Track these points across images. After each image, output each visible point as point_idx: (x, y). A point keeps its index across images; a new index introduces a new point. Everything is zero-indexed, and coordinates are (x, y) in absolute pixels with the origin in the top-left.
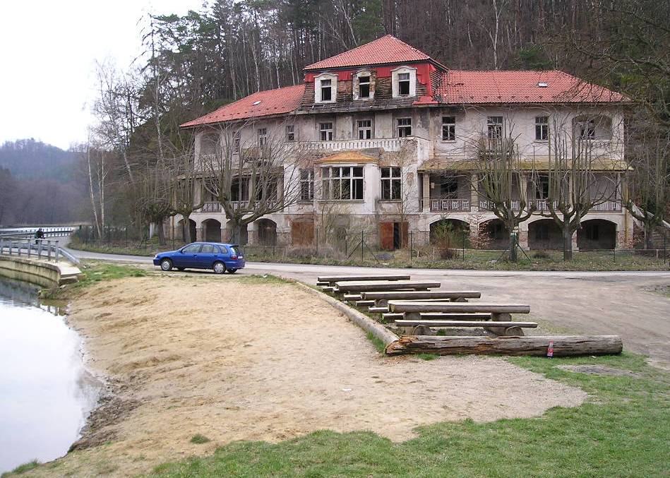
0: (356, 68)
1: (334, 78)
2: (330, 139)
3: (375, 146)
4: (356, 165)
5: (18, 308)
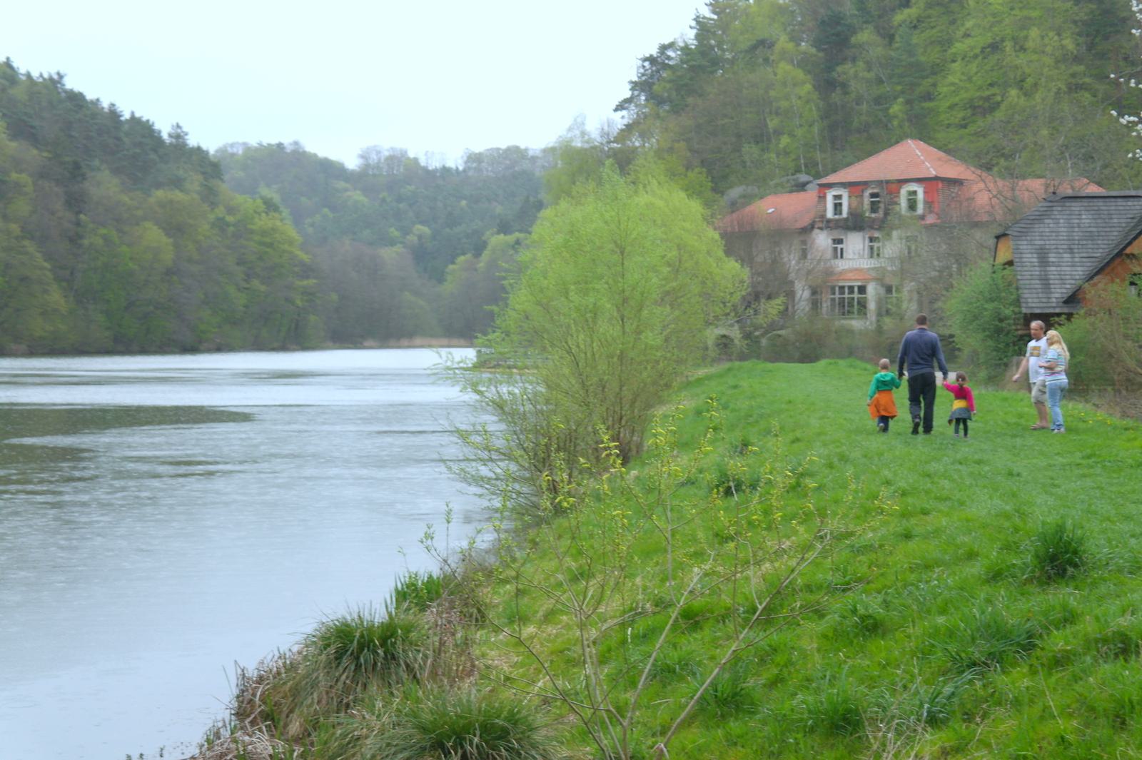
0: (865, 184)
1: (845, 194)
2: (842, 257)
4: (860, 284)
5: (523, 147)
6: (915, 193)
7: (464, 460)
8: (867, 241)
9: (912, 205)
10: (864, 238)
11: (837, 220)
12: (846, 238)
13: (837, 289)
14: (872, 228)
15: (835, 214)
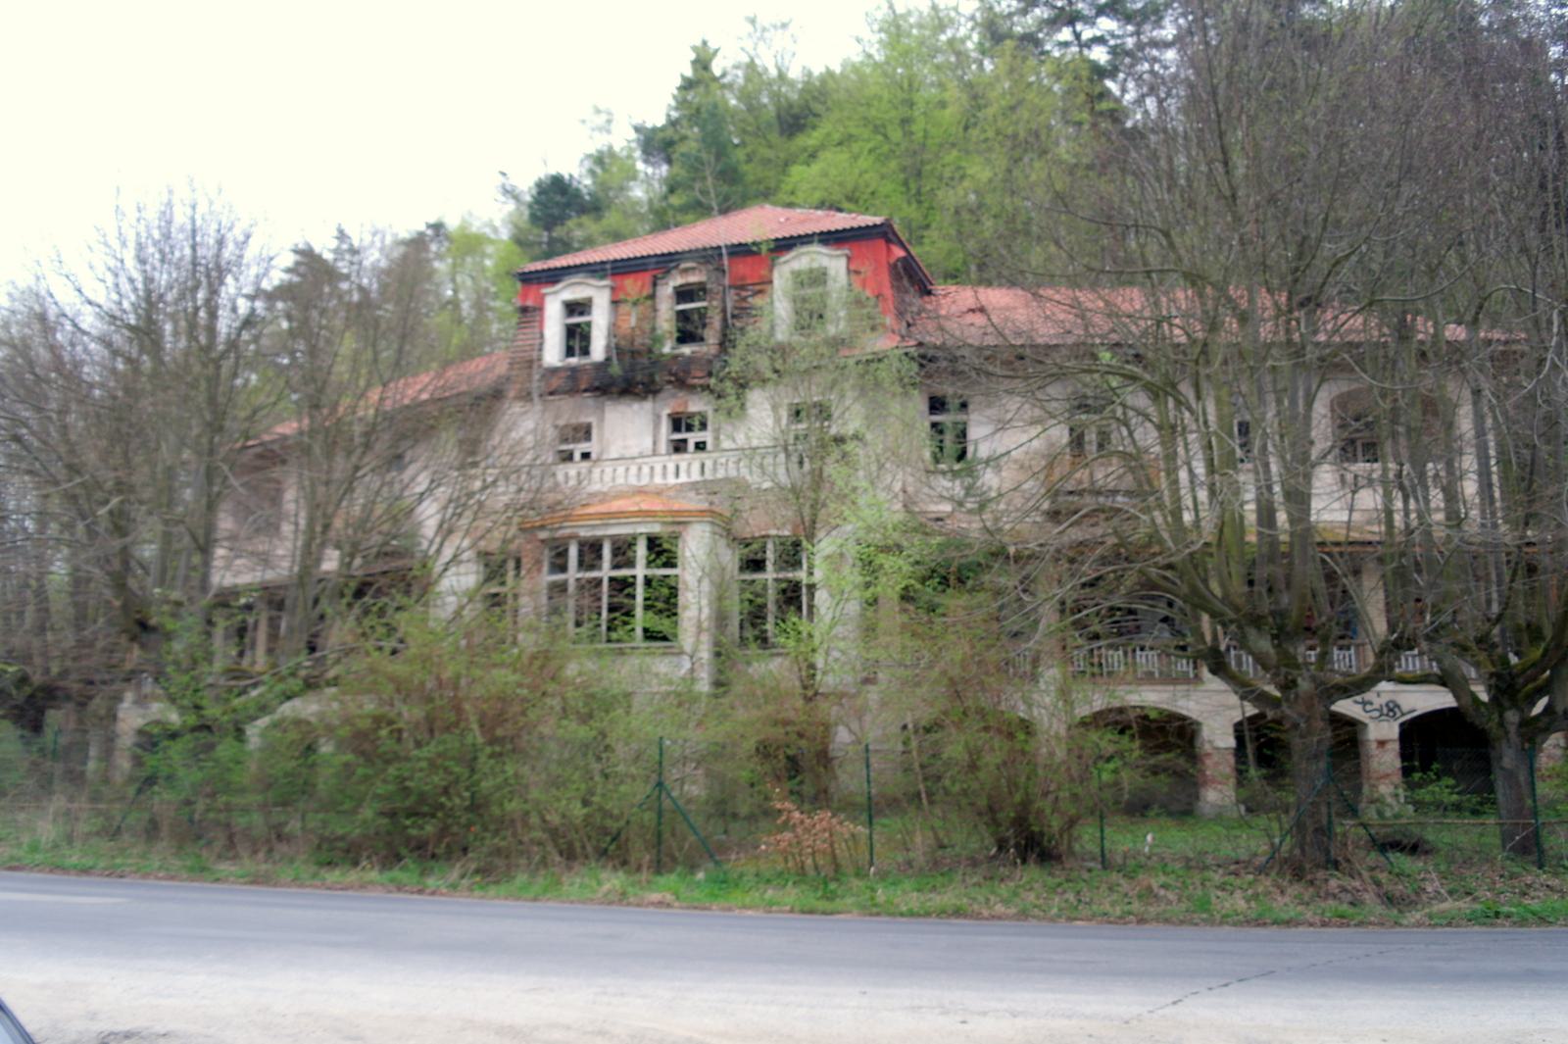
1: (599, 295)
3: (721, 474)
4: (655, 529)
6: (819, 277)
7: (661, 749)
8: (665, 426)
9: (810, 316)
10: (657, 418)
11: (574, 371)
12: (602, 420)
13: (573, 552)
14: (681, 383)
15: (570, 352)
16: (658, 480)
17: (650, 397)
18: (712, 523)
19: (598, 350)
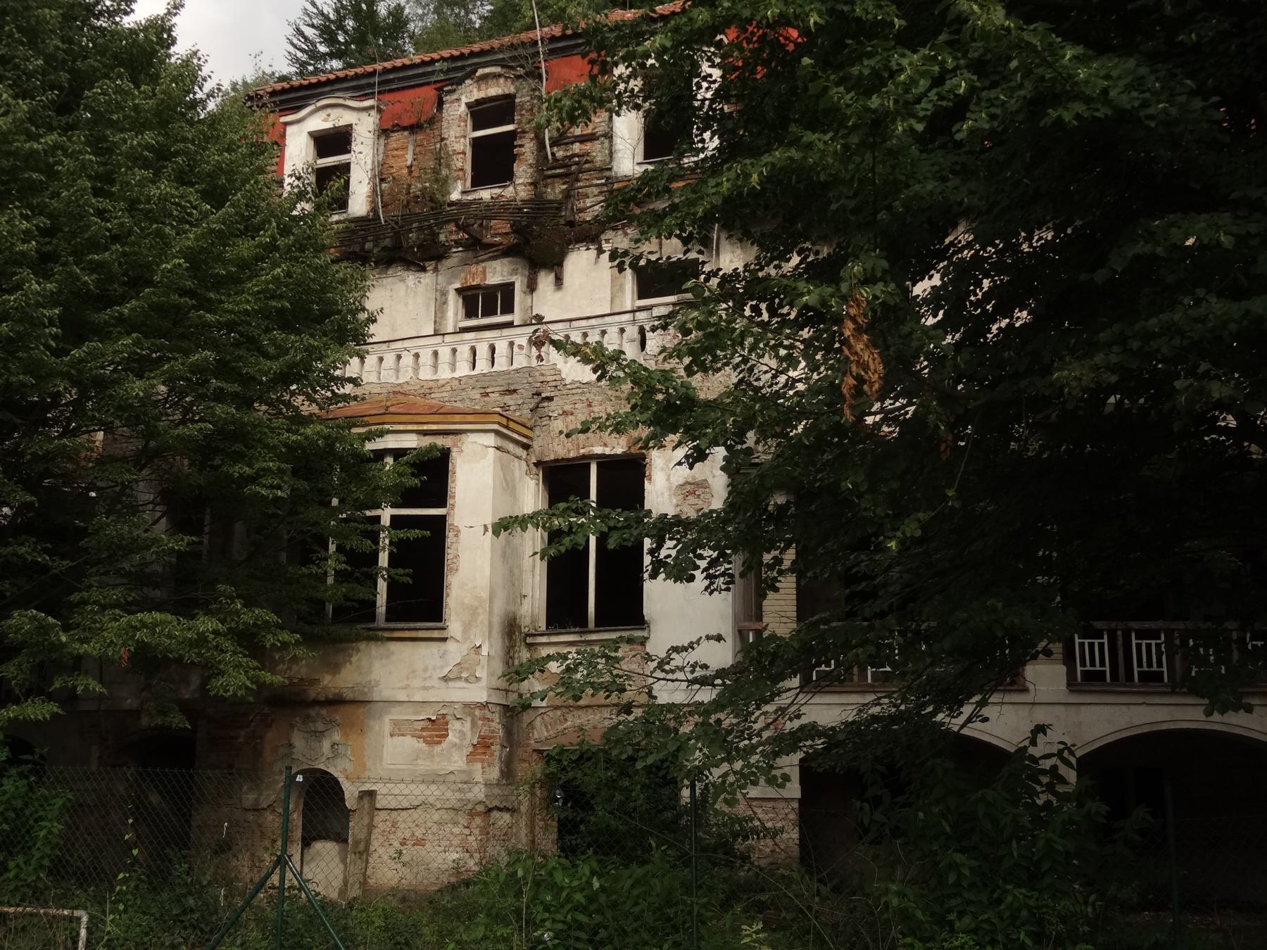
14: (477, 247)
16: (426, 374)
17: (430, 265)
18: (497, 432)
19: (359, 204)
